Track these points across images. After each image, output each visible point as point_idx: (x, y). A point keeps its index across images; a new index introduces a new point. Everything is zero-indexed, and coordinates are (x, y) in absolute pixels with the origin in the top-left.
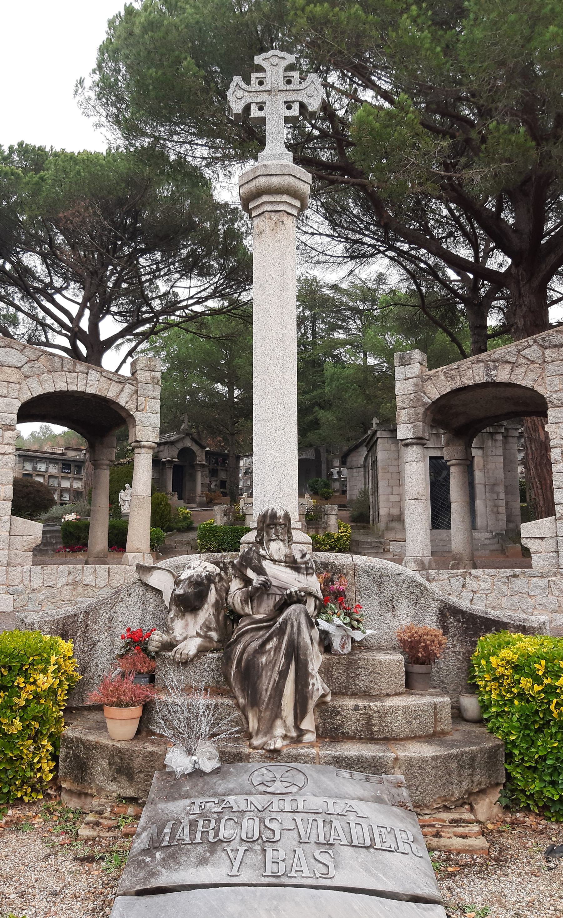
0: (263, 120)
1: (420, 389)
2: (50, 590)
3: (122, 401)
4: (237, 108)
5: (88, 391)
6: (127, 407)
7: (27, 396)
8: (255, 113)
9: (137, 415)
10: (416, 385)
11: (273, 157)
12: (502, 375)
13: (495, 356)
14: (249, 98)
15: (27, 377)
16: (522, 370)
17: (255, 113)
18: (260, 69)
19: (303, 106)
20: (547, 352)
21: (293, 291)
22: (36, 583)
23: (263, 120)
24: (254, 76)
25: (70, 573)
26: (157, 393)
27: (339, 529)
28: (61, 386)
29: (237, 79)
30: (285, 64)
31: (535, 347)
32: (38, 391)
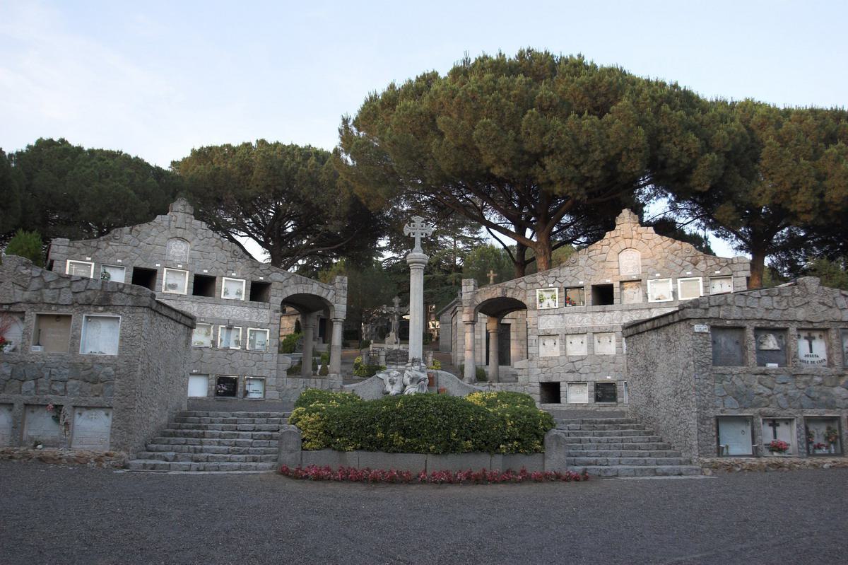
0: (414, 238)
1: (473, 298)
2: (295, 390)
3: (329, 298)
4: (406, 234)
5: (313, 293)
6: (331, 301)
7: (285, 296)
8: (412, 236)
9: (335, 305)
10: (472, 296)
11: (417, 251)
12: (509, 295)
13: (506, 285)
14: (410, 231)
15: (285, 287)
16: (517, 293)
17: (412, 236)
18: (413, 222)
19: (426, 234)
20: (528, 285)
21: (390, 82)
22: (289, 386)
23: (414, 238)
24: (412, 224)
25: (304, 383)
26: (345, 294)
27: (625, 383)
28: (301, 291)
29: (407, 225)
30: (421, 221)
31: (523, 283)
32: (290, 293)
